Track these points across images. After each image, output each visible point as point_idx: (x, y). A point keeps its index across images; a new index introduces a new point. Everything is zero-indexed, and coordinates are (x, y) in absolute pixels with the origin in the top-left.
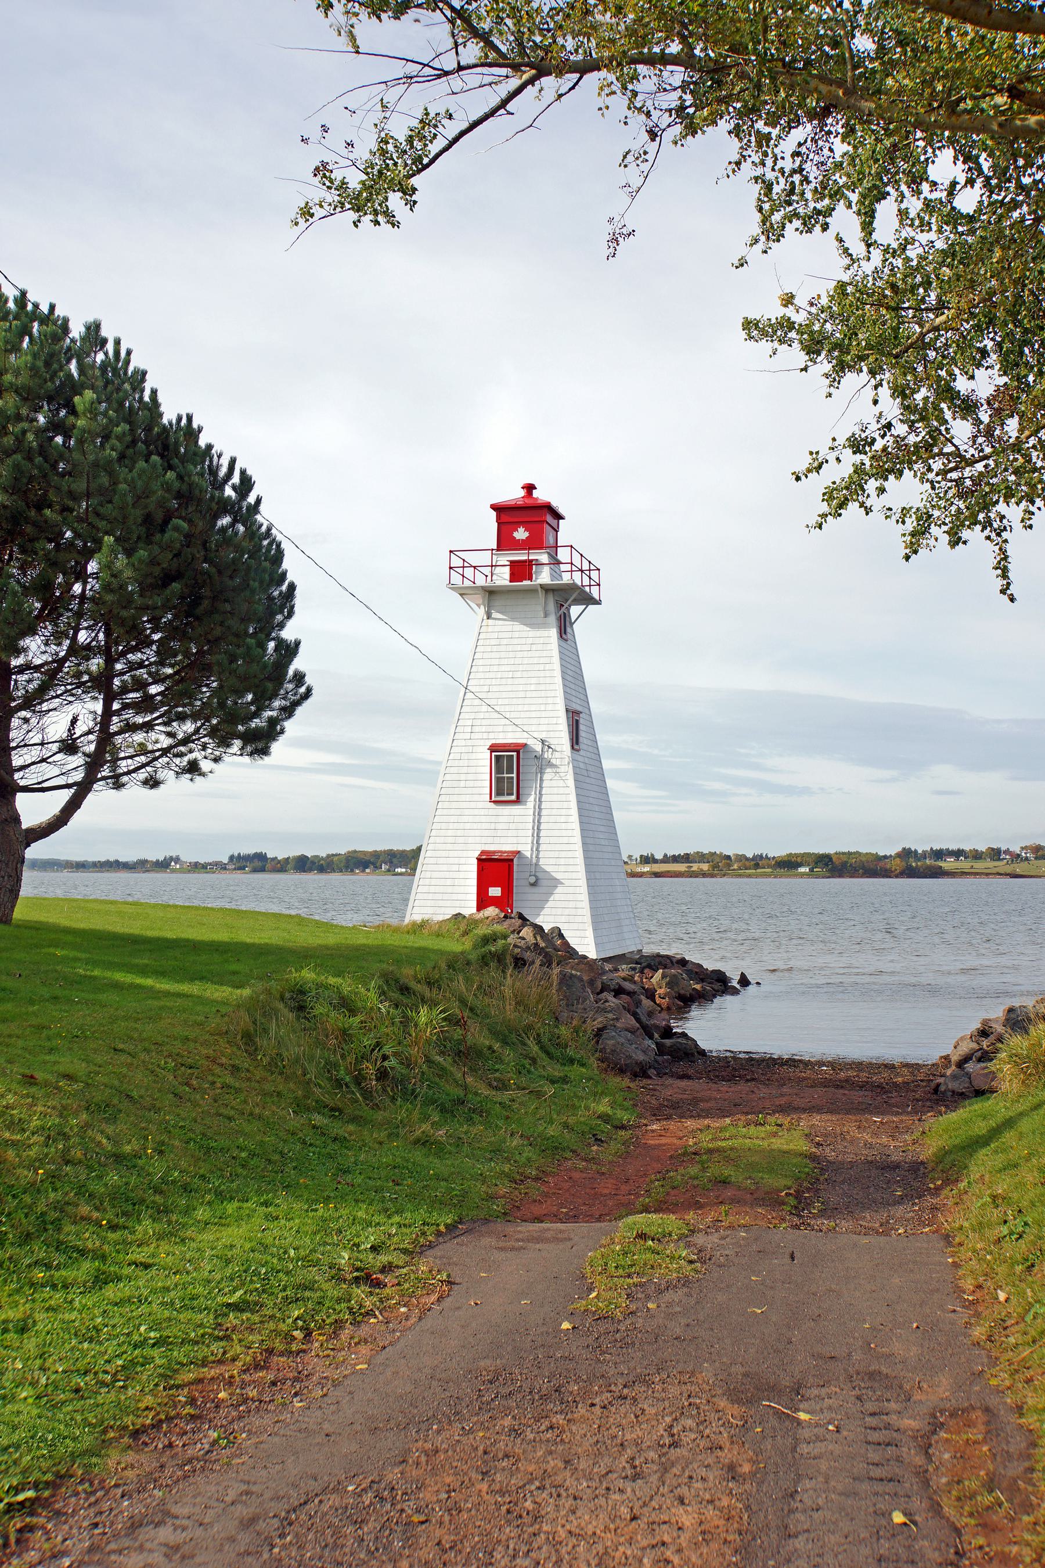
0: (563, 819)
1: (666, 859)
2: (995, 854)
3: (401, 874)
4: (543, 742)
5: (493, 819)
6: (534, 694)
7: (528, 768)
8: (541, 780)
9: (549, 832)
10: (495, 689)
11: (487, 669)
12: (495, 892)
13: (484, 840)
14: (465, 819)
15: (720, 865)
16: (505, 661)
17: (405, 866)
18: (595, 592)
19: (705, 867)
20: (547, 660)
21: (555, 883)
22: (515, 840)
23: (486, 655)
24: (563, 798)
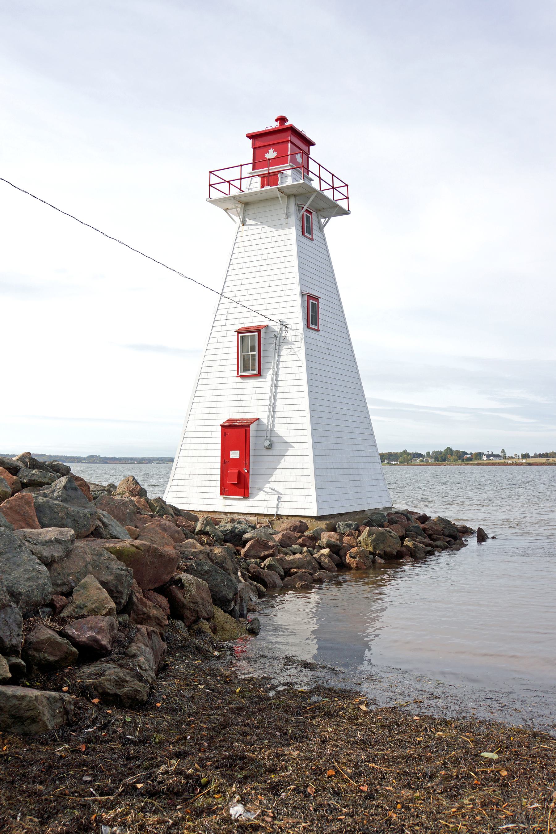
1: (536, 456)
3: (394, 465)
4: (281, 323)
7: (268, 347)
8: (279, 356)
9: (284, 401)
12: (235, 454)
17: (397, 460)
18: (343, 204)
21: (287, 446)
23: (241, 255)
24: (296, 370)
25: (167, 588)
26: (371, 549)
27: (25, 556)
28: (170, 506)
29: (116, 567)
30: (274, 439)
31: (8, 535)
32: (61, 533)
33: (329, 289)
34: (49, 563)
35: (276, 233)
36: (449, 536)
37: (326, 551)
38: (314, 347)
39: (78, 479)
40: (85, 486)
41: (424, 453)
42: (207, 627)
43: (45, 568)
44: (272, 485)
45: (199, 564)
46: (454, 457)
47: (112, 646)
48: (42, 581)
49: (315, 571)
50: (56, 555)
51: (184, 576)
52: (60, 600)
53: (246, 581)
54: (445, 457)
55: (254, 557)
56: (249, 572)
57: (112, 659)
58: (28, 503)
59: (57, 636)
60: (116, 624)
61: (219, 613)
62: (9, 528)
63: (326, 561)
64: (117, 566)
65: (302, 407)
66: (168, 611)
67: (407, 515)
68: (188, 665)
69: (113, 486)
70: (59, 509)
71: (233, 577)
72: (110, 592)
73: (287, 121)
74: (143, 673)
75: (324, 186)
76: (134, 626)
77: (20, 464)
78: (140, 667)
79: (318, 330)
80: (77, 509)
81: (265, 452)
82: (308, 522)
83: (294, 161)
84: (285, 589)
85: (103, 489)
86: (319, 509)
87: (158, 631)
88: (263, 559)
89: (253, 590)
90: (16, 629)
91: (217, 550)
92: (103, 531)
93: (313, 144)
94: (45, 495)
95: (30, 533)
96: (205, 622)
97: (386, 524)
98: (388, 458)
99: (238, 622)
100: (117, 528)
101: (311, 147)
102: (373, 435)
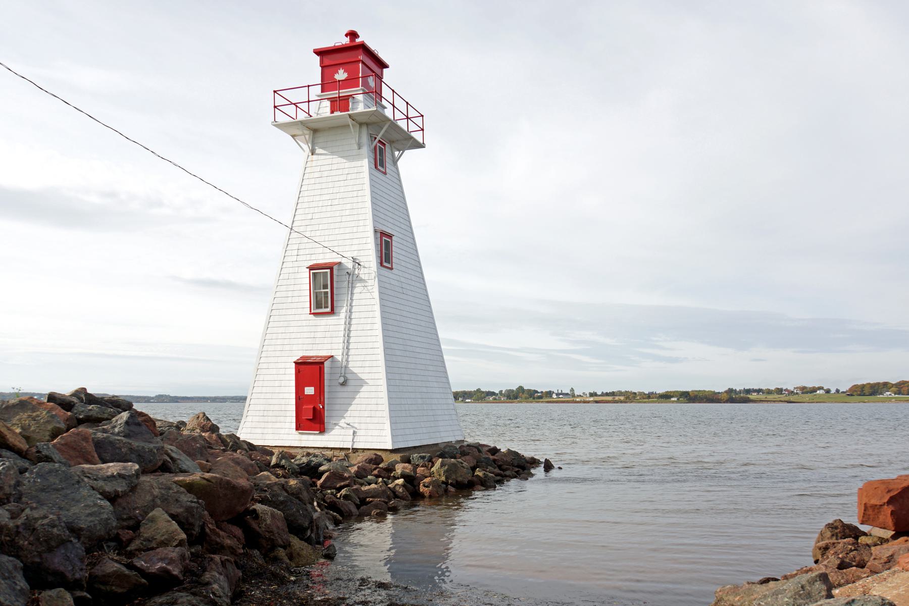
0: (369, 327)
1: (603, 395)
2: (779, 391)
4: (354, 260)
5: (313, 329)
6: (349, 218)
7: (341, 284)
8: (352, 294)
9: (359, 339)
10: (317, 216)
11: (311, 199)
13: (305, 347)
14: (291, 330)
15: (630, 397)
16: (326, 191)
18: (418, 136)
19: (622, 398)
20: (359, 187)
21: (362, 383)
22: (329, 346)
24: (370, 308)
25: (243, 519)
26: (443, 478)
27: (85, 492)
28: (244, 441)
29: (186, 499)
30: (348, 376)
31: (64, 472)
32: (125, 468)
33: (403, 226)
34: (113, 498)
35: (348, 164)
36: (518, 466)
37: (401, 481)
38: (387, 286)
39: (141, 414)
40: (149, 422)
41: (497, 392)
42: (284, 554)
43: (108, 503)
44: (348, 420)
45: (273, 496)
46: (525, 395)
47: (184, 576)
48: (105, 516)
49: (390, 500)
50: (120, 490)
51: (258, 507)
52: (126, 535)
53: (322, 510)
54: (516, 395)
55: (330, 488)
56: (325, 501)
57: (184, 588)
58: (85, 439)
59: (124, 569)
60: (188, 554)
61: (296, 542)
62: (65, 464)
63: (401, 490)
64: (187, 499)
65: (376, 345)
66: (243, 541)
67: (478, 447)
68: (264, 591)
69: (183, 423)
70: (121, 445)
71: (309, 507)
72: (180, 524)
73: (358, 36)
74: (217, 599)
75: (398, 115)
76: (207, 556)
77: (75, 400)
78: (214, 594)
79: (391, 269)
80: (142, 444)
81: (340, 388)
82: (384, 455)
83: (366, 84)
84: (360, 519)
85: (171, 425)
86: (393, 442)
87: (232, 560)
88: (339, 489)
89: (329, 519)
90: (79, 564)
91: (293, 482)
92: (172, 465)
93: (386, 66)
94: (105, 431)
95: (89, 468)
96: (281, 550)
97: (458, 455)
98: (457, 396)
99: (315, 549)
100: (186, 462)
101: (385, 70)
102: (446, 372)
